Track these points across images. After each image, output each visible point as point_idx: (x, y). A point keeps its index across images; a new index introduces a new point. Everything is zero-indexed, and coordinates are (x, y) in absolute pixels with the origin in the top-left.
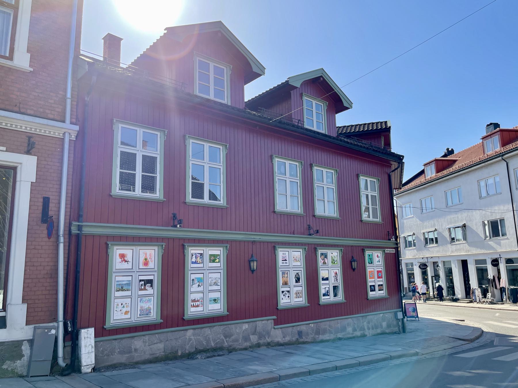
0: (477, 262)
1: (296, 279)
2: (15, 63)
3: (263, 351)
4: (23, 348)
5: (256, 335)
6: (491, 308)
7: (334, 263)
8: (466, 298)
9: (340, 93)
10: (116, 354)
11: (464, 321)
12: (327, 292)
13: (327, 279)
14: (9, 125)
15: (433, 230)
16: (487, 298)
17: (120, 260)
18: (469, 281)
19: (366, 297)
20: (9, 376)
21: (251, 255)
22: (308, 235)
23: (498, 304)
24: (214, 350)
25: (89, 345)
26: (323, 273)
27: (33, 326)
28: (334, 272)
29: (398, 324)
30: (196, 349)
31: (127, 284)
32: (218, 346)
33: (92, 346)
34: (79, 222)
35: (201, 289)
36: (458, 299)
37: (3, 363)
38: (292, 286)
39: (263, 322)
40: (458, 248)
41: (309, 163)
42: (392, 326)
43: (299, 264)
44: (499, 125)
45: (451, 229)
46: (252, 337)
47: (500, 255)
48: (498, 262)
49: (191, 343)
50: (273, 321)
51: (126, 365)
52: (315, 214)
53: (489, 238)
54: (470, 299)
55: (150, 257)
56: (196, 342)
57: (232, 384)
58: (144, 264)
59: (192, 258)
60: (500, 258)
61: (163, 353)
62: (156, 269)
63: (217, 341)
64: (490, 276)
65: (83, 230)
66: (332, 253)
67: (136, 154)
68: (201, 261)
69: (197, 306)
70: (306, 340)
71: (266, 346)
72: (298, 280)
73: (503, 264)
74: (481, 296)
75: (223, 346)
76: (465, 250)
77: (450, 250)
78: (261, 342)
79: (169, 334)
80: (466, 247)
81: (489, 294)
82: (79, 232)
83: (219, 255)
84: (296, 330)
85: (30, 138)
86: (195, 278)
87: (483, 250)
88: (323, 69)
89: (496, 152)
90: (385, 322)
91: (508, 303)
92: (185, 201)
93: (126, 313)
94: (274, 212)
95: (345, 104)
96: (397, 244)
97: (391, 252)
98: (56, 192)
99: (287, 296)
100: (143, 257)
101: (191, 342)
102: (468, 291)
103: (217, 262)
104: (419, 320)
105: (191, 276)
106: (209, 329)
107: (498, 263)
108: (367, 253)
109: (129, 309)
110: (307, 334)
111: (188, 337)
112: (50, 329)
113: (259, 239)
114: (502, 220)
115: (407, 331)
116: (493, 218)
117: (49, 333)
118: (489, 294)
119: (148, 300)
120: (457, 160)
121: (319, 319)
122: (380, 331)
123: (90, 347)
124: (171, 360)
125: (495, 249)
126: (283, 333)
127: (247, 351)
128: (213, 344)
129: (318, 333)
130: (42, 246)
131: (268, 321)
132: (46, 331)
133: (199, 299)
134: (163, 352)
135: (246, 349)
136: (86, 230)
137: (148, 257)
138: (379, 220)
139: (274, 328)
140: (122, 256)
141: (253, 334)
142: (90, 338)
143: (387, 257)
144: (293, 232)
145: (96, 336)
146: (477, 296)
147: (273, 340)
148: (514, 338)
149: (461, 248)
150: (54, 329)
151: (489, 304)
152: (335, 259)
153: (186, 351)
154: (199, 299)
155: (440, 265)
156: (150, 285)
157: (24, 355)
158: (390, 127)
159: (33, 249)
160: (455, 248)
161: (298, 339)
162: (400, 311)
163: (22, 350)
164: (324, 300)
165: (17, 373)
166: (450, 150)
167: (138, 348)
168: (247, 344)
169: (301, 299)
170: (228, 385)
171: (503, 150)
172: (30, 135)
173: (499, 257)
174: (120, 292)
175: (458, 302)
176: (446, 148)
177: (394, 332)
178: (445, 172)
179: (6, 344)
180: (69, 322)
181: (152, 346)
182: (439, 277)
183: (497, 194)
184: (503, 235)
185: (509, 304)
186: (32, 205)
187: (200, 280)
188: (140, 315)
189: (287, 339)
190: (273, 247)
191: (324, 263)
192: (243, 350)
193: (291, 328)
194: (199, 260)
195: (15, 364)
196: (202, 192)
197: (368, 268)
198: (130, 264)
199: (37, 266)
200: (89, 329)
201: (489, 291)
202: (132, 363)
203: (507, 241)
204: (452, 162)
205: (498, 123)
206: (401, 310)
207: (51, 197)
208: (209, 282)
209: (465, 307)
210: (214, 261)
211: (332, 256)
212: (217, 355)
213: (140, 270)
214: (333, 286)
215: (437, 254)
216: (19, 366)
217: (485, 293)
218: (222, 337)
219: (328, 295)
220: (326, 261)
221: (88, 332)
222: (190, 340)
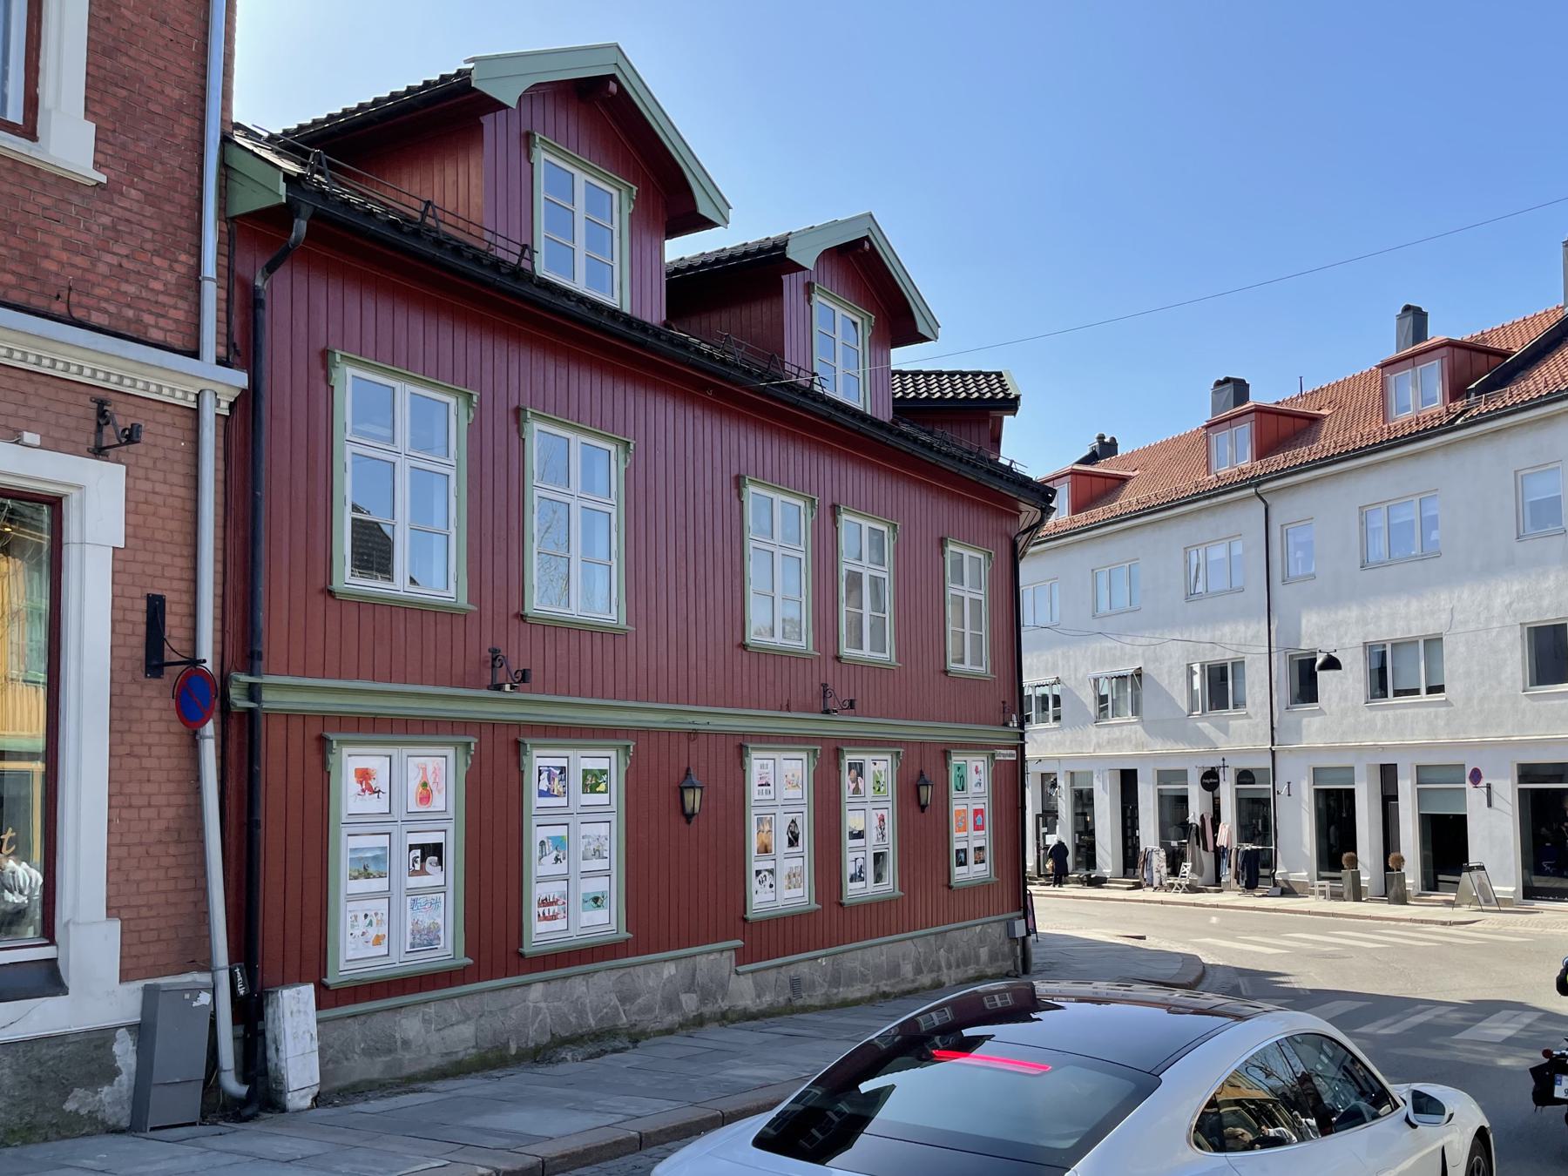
0: (1163, 777)
1: (789, 838)
2: (52, 152)
3: (715, 1035)
4: (117, 1049)
5: (695, 992)
6: (1193, 902)
7: (879, 790)
8: (1125, 875)
9: (669, 139)
10: (356, 1057)
11: (1143, 938)
12: (861, 871)
13: (859, 835)
14: (32, 359)
15: (1051, 680)
16: (1182, 877)
17: (358, 788)
18: (1135, 827)
19: (946, 882)
20: (84, 1132)
21: (684, 772)
22: (822, 713)
23: (1208, 892)
24: (597, 1036)
25: (304, 1033)
26: (853, 821)
27: (140, 984)
28: (877, 815)
29: (1013, 950)
30: (553, 1035)
31: (375, 858)
32: (605, 1025)
33: (312, 1035)
34: (251, 674)
35: (561, 868)
36: (1104, 880)
37: (65, 1094)
38: (780, 857)
39: (712, 957)
40: (1115, 736)
41: (828, 503)
42: (1000, 957)
43: (797, 793)
44: (1249, 385)
45: (1101, 681)
46: (684, 998)
47: (1224, 760)
48: (1218, 777)
49: (541, 1021)
50: (733, 952)
51: (384, 1085)
52: (841, 653)
53: (1200, 712)
54: (1134, 878)
55: (435, 779)
56: (551, 1015)
57: (739, 1108)
58: (421, 799)
59: (539, 780)
60: (1224, 767)
61: (474, 1051)
62: (451, 815)
63: (602, 1014)
64: (1194, 817)
65: (263, 698)
66: (875, 764)
67: (861, 574)
68: (561, 790)
69: (554, 917)
70: (809, 1002)
71: (717, 1021)
72: (793, 841)
73: (1228, 784)
74: (1164, 870)
75: (617, 1025)
76: (1134, 742)
77: (1094, 741)
78: (707, 1010)
79: (486, 996)
80: (1138, 736)
81: (1186, 866)
82: (252, 705)
83: (604, 772)
84: (785, 975)
85: (101, 403)
86: (548, 838)
87: (1181, 744)
88: (871, 216)
89: (1242, 472)
90: (986, 948)
91: (1234, 890)
92: (521, 613)
93: (378, 940)
94: (744, 646)
95: (922, 328)
96: (1022, 736)
97: (1008, 758)
98: (182, 579)
99: (767, 883)
100: (416, 778)
101: (540, 1017)
102: (1131, 858)
103: (602, 792)
104: (1037, 941)
105: (537, 834)
106: (583, 980)
107: (1216, 781)
108: (956, 760)
109: (384, 930)
110: (812, 986)
111: (531, 1005)
112: (195, 991)
113: (704, 724)
114: (1239, 665)
115: (1033, 968)
116: (1217, 656)
117: (195, 1004)
118: (1186, 866)
119: (432, 904)
120: (1130, 477)
121: (698, 945)
122: (973, 971)
123: (308, 1037)
124: (494, 1068)
125: (1213, 742)
126: (756, 984)
127: (672, 1036)
128: (594, 1020)
129: (836, 981)
130: (150, 746)
131: (722, 955)
132: (187, 996)
133: (556, 897)
134: (473, 1047)
135: (670, 1031)
136: (271, 700)
137: (429, 777)
138: (983, 669)
139: (737, 973)
140: (364, 776)
141: (689, 990)
142: (305, 1012)
143: (997, 768)
144: (788, 705)
145: (320, 1006)
146: (1154, 870)
147: (733, 1006)
148: (1282, 979)
149: (1123, 736)
150: (206, 990)
151: (1184, 892)
152: (882, 780)
153: (529, 1043)
154: (556, 897)
155: (1061, 782)
156: (436, 858)
157: (119, 1069)
158: (1017, 398)
159: (127, 754)
160: (1106, 737)
161: (790, 1000)
162: (1020, 918)
163: (113, 1057)
164: (854, 891)
165: (103, 1122)
166: (1107, 440)
167: (411, 1038)
168: (673, 1019)
169: (799, 892)
170: (730, 1113)
171: (1260, 468)
172: (101, 394)
173: (1221, 764)
174: (363, 881)
175: (1103, 887)
176: (1097, 435)
177: (1004, 972)
178: (1099, 513)
179: (71, 1039)
180: (238, 970)
181: (446, 1032)
182: (1057, 817)
183: (1232, 591)
184: (1236, 706)
185: (1236, 890)
186: (117, 620)
187: (559, 843)
188: (413, 946)
189: (768, 999)
190: (740, 748)
191: (856, 790)
192: (664, 1035)
193: (774, 972)
194: (557, 786)
195: (97, 1098)
196: (358, 533)
197: (954, 802)
198: (385, 797)
199: (139, 808)
200: (303, 988)
201: (1189, 856)
202: (398, 1081)
203: (1245, 722)
204: (1117, 482)
205: (1244, 381)
206: (1020, 913)
207: (169, 596)
208: (582, 849)
209: (1125, 900)
210: (593, 790)
211: (874, 772)
212: (610, 1049)
213: (412, 818)
214: (875, 854)
215: (1056, 751)
216: (109, 1103)
217: (1174, 861)
218: (615, 1001)
219: (863, 880)
220: (861, 786)
221: (300, 996)
222: (537, 1011)
